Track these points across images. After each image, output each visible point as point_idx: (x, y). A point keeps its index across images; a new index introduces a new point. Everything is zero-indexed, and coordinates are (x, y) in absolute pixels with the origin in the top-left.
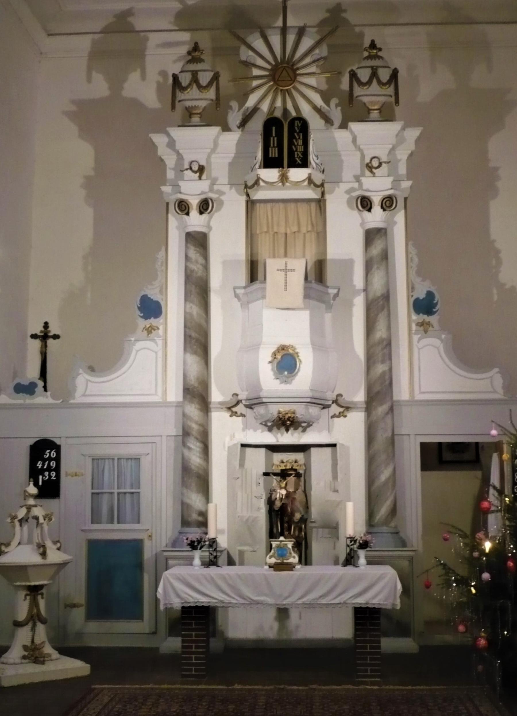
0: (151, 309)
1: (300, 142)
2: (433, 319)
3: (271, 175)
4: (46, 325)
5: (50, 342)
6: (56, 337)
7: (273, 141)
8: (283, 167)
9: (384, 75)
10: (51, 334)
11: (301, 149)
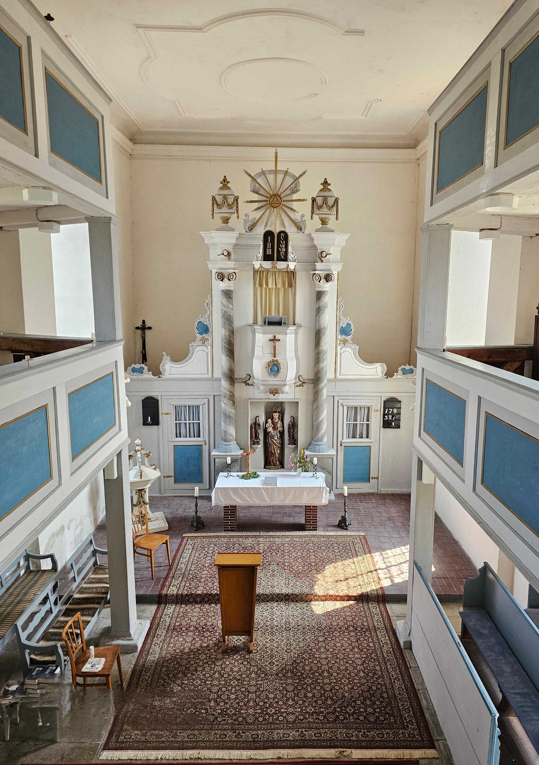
0: (205, 329)
1: (284, 246)
2: (349, 338)
3: (267, 265)
4: (144, 322)
5: (147, 332)
6: (150, 328)
7: (269, 245)
9: (231, 200)
10: (147, 326)
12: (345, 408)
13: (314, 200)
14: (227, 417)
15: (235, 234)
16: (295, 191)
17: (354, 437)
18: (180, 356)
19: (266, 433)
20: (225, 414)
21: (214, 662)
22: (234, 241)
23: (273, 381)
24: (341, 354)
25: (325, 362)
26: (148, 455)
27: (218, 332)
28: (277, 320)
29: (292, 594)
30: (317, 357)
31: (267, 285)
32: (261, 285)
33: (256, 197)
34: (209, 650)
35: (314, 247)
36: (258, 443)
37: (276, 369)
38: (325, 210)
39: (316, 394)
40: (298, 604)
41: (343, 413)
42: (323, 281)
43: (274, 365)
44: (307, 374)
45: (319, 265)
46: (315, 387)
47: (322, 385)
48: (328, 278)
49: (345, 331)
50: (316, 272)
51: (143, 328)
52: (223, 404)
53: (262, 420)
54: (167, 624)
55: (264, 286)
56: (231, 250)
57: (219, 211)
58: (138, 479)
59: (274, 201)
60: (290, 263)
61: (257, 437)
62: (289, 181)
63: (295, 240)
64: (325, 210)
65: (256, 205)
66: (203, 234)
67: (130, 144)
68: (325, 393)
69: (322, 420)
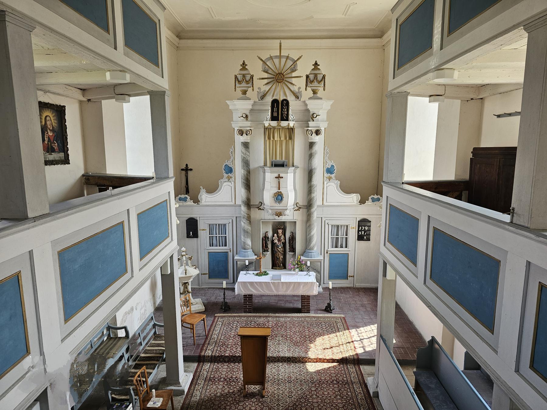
0: (230, 170)
2: (333, 176)
3: (274, 123)
4: (187, 165)
5: (189, 172)
6: (191, 170)
7: (275, 109)
8: (278, 120)
9: (248, 78)
11: (286, 113)
12: (330, 226)
13: (307, 77)
14: (246, 232)
15: (251, 102)
16: (294, 70)
17: (336, 247)
18: (212, 189)
19: (273, 244)
20: (244, 230)
21: (238, 403)
22: (251, 107)
23: (278, 207)
24: (327, 187)
25: (316, 193)
26: (190, 259)
27: (239, 172)
28: (281, 163)
29: (292, 357)
30: (310, 190)
31: (274, 138)
32: (269, 138)
33: (266, 75)
34: (234, 395)
35: (308, 110)
36: (267, 251)
37: (280, 198)
38: (315, 84)
39: (309, 216)
40: (297, 364)
41: (328, 230)
42: (314, 134)
43: (279, 195)
44: (302, 202)
45: (311, 123)
46: (308, 211)
47: (313, 210)
48: (318, 132)
49: (330, 171)
50: (309, 128)
51: (187, 170)
52: (242, 223)
53: (270, 234)
54: (205, 376)
55: (272, 139)
56: (248, 114)
57: (240, 86)
58: (184, 276)
59: (279, 78)
60: (290, 122)
61: (266, 247)
62: (290, 63)
63: (294, 106)
64: (315, 84)
65: (266, 81)
66: (228, 102)
67: (177, 39)
68: (316, 213)
69: (313, 235)
